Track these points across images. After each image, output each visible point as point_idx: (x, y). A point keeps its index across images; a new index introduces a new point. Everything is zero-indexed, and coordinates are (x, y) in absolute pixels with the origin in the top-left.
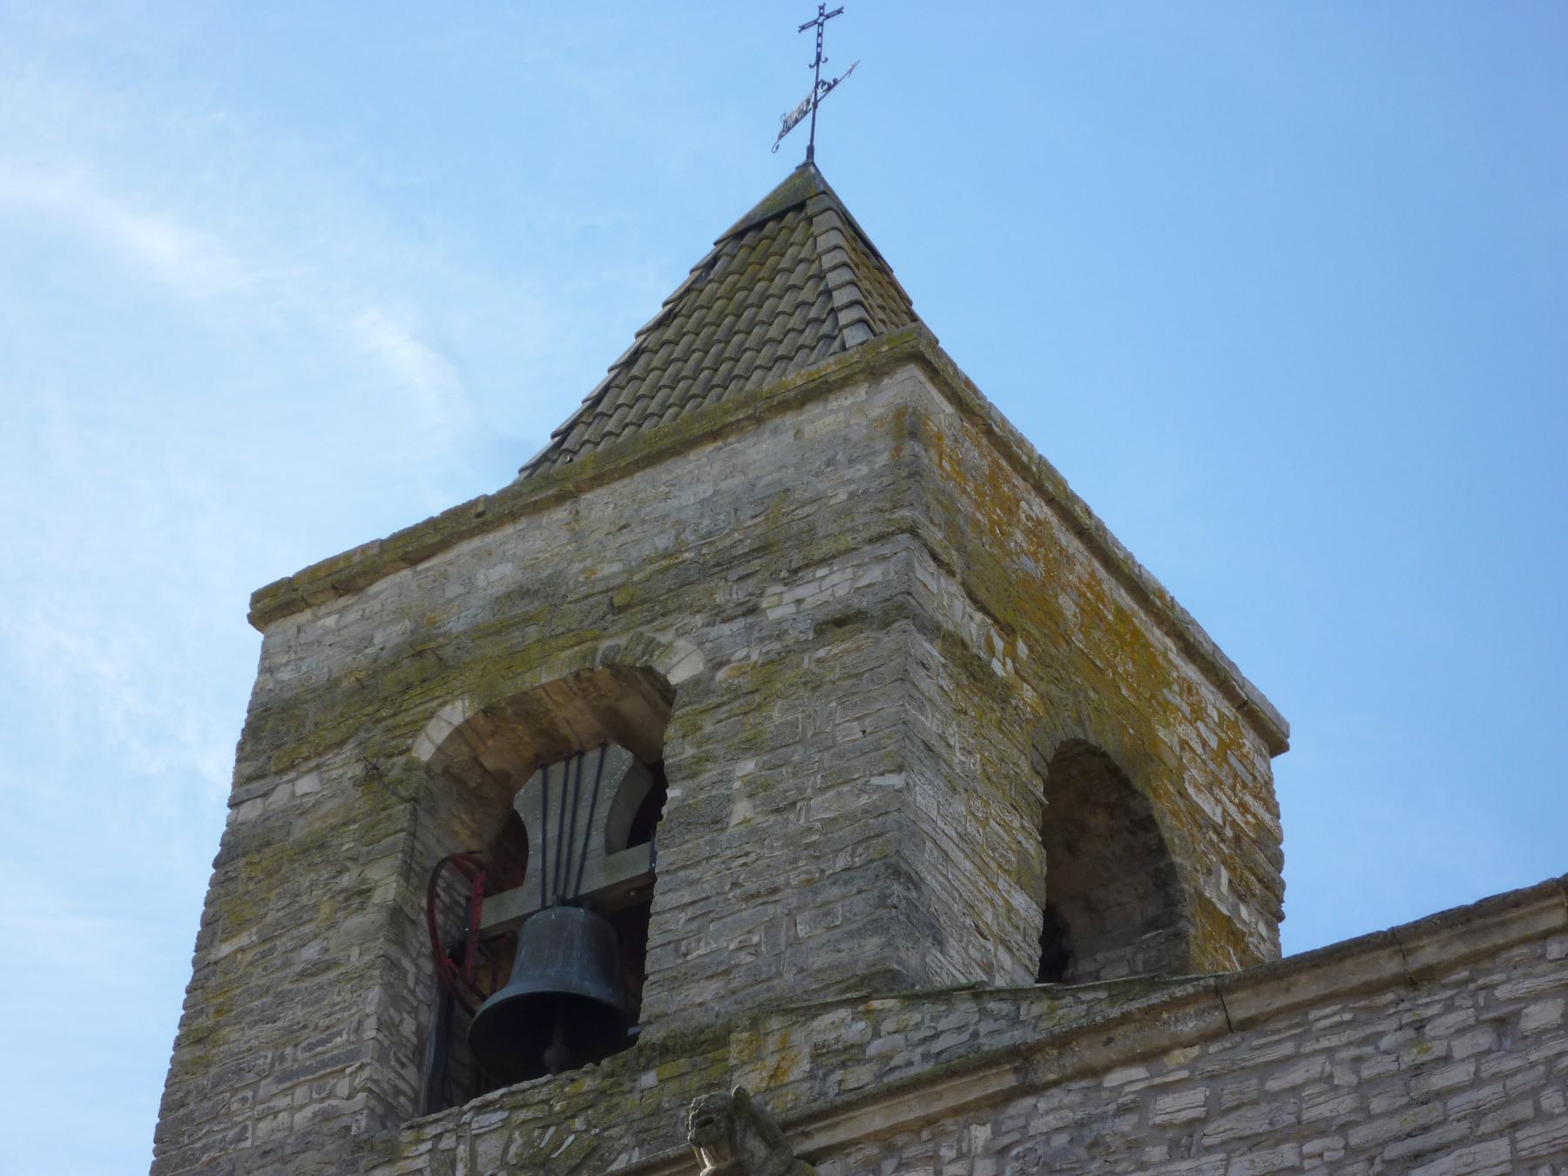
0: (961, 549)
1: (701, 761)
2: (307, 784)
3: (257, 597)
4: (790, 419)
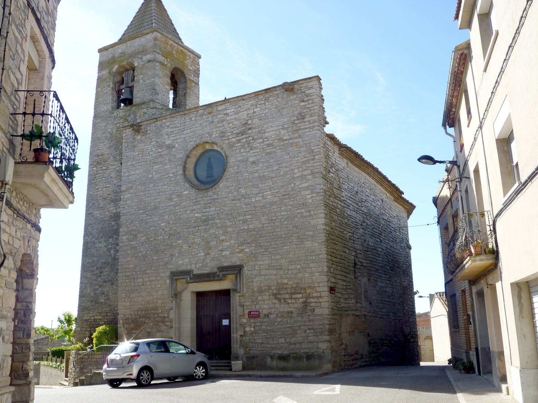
0: (161, 51)
1: (138, 75)
2: (104, 72)
3: (98, 50)
4: (145, 36)
